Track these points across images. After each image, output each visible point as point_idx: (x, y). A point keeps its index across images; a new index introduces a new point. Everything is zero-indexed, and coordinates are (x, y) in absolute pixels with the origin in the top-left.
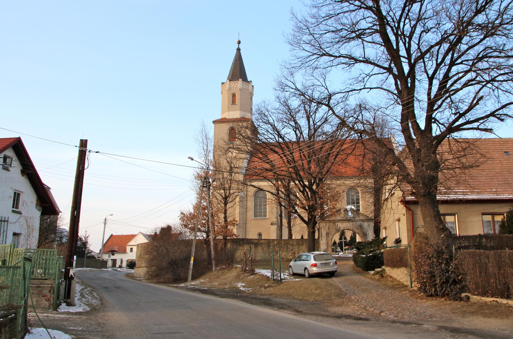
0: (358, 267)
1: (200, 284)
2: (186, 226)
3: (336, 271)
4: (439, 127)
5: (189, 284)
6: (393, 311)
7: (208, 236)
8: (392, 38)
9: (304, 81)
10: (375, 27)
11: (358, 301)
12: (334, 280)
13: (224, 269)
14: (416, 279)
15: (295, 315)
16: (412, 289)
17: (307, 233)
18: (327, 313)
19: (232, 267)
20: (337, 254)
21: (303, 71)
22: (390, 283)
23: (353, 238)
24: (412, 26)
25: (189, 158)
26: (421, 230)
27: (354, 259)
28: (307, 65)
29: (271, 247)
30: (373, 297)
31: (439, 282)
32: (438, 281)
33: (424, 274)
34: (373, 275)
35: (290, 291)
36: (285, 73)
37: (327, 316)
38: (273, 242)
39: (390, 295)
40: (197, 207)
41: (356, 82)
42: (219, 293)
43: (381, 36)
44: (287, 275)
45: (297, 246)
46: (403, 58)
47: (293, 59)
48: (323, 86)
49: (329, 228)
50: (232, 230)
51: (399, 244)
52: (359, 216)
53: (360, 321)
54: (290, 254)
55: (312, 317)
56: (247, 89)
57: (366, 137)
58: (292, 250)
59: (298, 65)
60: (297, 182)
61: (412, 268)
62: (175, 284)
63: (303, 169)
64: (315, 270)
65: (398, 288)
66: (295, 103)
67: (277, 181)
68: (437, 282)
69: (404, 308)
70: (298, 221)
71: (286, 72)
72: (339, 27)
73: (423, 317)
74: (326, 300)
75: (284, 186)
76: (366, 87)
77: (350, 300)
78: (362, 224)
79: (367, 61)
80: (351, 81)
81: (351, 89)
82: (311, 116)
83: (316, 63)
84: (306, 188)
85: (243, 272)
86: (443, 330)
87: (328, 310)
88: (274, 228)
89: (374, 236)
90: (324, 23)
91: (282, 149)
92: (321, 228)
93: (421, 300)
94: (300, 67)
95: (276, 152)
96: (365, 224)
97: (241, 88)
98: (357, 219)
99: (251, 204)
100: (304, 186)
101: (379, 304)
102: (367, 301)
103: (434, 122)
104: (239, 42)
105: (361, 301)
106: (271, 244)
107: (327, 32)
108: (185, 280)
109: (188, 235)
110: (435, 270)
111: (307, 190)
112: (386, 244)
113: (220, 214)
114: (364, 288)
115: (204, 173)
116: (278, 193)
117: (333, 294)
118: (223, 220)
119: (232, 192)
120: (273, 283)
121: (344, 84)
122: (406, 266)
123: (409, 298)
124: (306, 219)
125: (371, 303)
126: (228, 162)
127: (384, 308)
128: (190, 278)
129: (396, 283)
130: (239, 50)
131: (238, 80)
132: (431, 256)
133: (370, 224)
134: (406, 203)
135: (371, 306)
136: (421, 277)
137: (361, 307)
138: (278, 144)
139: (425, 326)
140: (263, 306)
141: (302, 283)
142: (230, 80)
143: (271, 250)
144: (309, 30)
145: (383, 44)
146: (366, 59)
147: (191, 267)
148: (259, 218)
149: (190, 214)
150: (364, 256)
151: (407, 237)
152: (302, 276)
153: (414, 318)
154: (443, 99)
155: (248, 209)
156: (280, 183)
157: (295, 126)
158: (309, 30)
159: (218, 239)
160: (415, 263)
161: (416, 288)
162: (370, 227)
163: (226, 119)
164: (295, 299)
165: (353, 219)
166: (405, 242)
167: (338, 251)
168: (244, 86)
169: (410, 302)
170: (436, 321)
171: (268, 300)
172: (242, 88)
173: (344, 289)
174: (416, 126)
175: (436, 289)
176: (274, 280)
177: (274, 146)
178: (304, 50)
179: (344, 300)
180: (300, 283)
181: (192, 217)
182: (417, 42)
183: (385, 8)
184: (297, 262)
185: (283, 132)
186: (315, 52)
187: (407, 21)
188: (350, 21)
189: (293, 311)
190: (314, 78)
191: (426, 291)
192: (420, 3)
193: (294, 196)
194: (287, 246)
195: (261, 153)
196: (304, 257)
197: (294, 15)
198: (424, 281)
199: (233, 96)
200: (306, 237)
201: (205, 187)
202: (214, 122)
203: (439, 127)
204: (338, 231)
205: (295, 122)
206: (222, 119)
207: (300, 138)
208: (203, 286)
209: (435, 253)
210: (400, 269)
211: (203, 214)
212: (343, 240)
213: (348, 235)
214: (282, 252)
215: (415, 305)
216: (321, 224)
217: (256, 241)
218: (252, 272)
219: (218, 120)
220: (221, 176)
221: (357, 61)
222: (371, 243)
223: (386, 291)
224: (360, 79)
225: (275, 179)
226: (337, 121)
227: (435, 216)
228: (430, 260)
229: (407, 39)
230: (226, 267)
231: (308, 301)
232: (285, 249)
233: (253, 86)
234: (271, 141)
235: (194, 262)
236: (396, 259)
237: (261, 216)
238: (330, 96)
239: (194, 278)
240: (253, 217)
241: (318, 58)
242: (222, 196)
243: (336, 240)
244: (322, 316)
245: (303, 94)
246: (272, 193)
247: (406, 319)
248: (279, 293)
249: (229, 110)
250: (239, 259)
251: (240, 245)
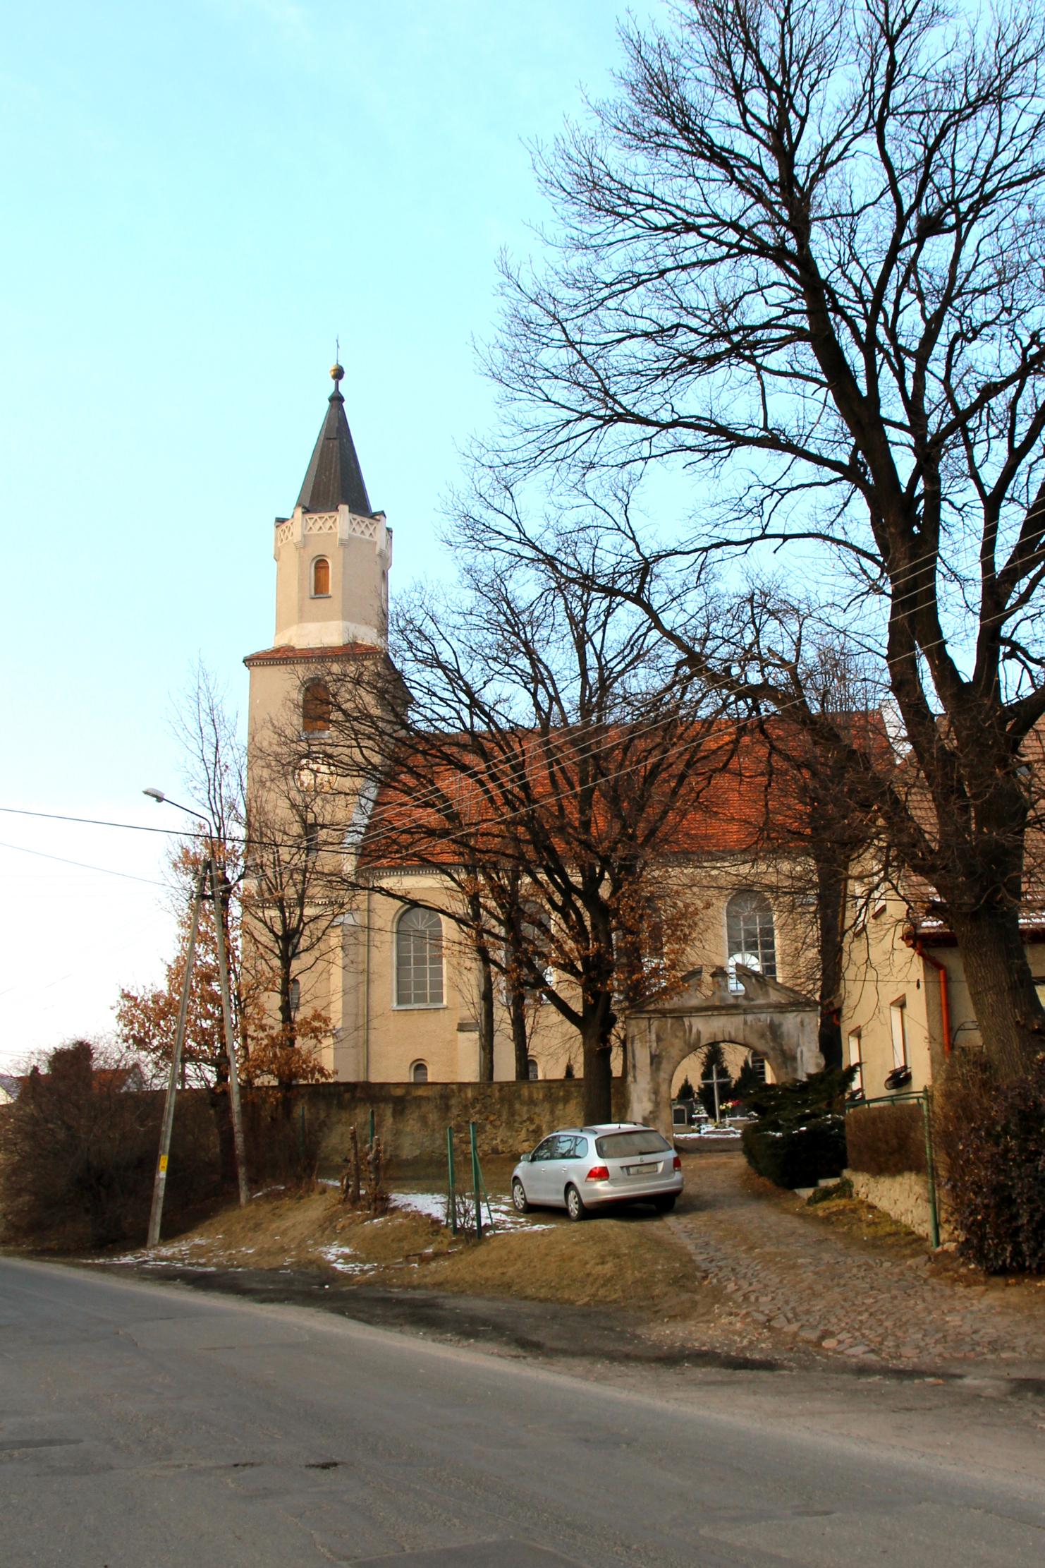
0: (761, 1174)
1: (192, 1255)
2: (141, 1043)
3: (677, 1193)
4: (1030, 671)
5: (152, 1254)
6: (867, 1332)
7: (222, 1077)
8: (855, 358)
9: (553, 513)
10: (792, 319)
11: (746, 1297)
12: (672, 1227)
13: (278, 1196)
14: (952, 1214)
15: (516, 1357)
16: (939, 1249)
17: (581, 1059)
18: (628, 1348)
19: (310, 1190)
20: (693, 1131)
21: (545, 474)
22: (865, 1230)
23: (752, 1074)
24: (928, 316)
25: (146, 793)
26: (974, 1038)
27: (746, 1146)
28: (560, 452)
29: (455, 1112)
30: (802, 1281)
31: (1029, 1222)
32: (1024, 1220)
33: (975, 1193)
34: (812, 1201)
35: (511, 1271)
36: (483, 482)
37: (627, 1358)
38: (460, 1091)
39: (862, 1273)
40: (182, 972)
41: (736, 515)
42: (254, 1285)
43: (818, 354)
44: (506, 1213)
45: (547, 1106)
46: (898, 431)
47: (509, 434)
48: (619, 529)
49: (659, 1039)
50: (310, 1052)
51: (904, 1090)
52: (767, 994)
53: (741, 1374)
54: (523, 1134)
55: (574, 1362)
56: (369, 542)
57: (768, 707)
58: (531, 1120)
59: (526, 455)
60: (542, 877)
61: (938, 1175)
62: (99, 1257)
63: (561, 830)
64: (604, 1190)
65: (892, 1246)
66: (757, 591)
67: (471, 870)
68: (1020, 1222)
69: (904, 1319)
70: (552, 1015)
71: (487, 481)
72: (669, 319)
73: (967, 1348)
74: (633, 1301)
75: (498, 892)
76: (768, 532)
77: (718, 1295)
78: (776, 1022)
79: (772, 440)
80: (714, 514)
81: (715, 541)
82: (590, 639)
83: (592, 446)
84: (574, 897)
85: (348, 1206)
86: (1030, 1395)
87: (638, 1337)
88: (470, 1041)
89: (822, 1062)
90: (611, 303)
91: (485, 755)
92: (633, 1037)
93: (968, 1286)
94: (533, 463)
95: (464, 768)
96: (790, 1022)
97: (346, 537)
98: (761, 1001)
99: (385, 954)
100: (568, 890)
101: (819, 1305)
102: (780, 1296)
103: (1008, 656)
104: (339, 374)
105: (757, 1299)
106: (453, 1102)
107: (624, 335)
108: (139, 1240)
109: (156, 1077)
110: (1012, 1179)
111: (579, 903)
112: (861, 1090)
113: (264, 997)
114: (773, 1249)
115: (206, 847)
116: (477, 916)
117: (659, 1276)
118: (279, 1016)
119: (309, 911)
120: (452, 1244)
121: (692, 523)
122: (916, 1166)
123: (925, 1281)
124: (577, 1007)
125: (792, 1304)
126: (293, 806)
127: (834, 1320)
128: (155, 1232)
129: (888, 1229)
130: (337, 400)
131: (337, 510)
132: (999, 1128)
133: (807, 1021)
134: (915, 939)
135: (790, 1315)
136: (968, 1206)
137: (754, 1321)
138: (467, 739)
139: (968, 1381)
140: (407, 1328)
141: (552, 1238)
142: (307, 511)
143: (453, 1123)
144: (564, 330)
145: (823, 378)
146: (770, 431)
147: (160, 1191)
148: (416, 1006)
149: (156, 998)
150: (778, 1134)
151: (928, 1062)
152: (556, 1212)
153: (935, 1353)
154: (1031, 575)
155: (373, 977)
156: (481, 878)
157: (530, 671)
158: (564, 330)
159: (259, 1088)
160: (949, 1154)
161: (951, 1246)
162: (808, 1029)
163: (292, 649)
164: (526, 1298)
165: (744, 1002)
166: (921, 1078)
167: (698, 1120)
168: (359, 530)
169: (928, 1296)
170: (1009, 1363)
171: (430, 1304)
172: (351, 538)
173: (699, 1258)
174: (945, 670)
175: (1017, 1246)
176: (456, 1231)
177: (457, 744)
178: (549, 400)
179: (698, 1297)
180: (546, 1240)
181: (162, 1010)
182: (942, 375)
183: (834, 251)
184: (538, 1164)
185: (487, 696)
186: (585, 409)
187: (907, 297)
188: (712, 299)
189: (507, 1344)
190: (585, 501)
191: (985, 1257)
192: (954, 234)
193: (532, 923)
194: (511, 1106)
195: (411, 771)
196: (564, 1147)
197: (509, 276)
198: (975, 1220)
199: (316, 568)
200: (579, 1073)
201: (207, 897)
202: (249, 661)
203: (1030, 671)
204: (693, 1047)
205: (531, 659)
206: (277, 650)
207: (548, 714)
208: (202, 1261)
209: (1014, 1120)
210: (899, 1179)
211: (202, 997)
212: (714, 1079)
213: (735, 1060)
214: (495, 1127)
215: (945, 1307)
216: (633, 1022)
217: (399, 1092)
218: (381, 1205)
219: (265, 652)
220: (268, 857)
221: (738, 440)
222: (804, 1088)
223: (849, 1261)
224: (748, 503)
225: (466, 867)
226: (672, 655)
227: (1013, 988)
228: (997, 1145)
229: (910, 364)
230: (288, 1189)
231: (572, 1303)
232: (504, 1117)
233: (389, 530)
234: (448, 730)
235: (168, 1174)
236: (887, 1142)
237: (421, 998)
238: (645, 569)
239: (169, 1234)
240: (395, 1004)
241: (596, 429)
242: (272, 931)
243: (691, 1081)
244: (612, 1357)
245: (550, 561)
246: (460, 921)
247: (910, 1356)
248: (469, 1278)
249: (302, 617)
250: (338, 1159)
251: (341, 1106)
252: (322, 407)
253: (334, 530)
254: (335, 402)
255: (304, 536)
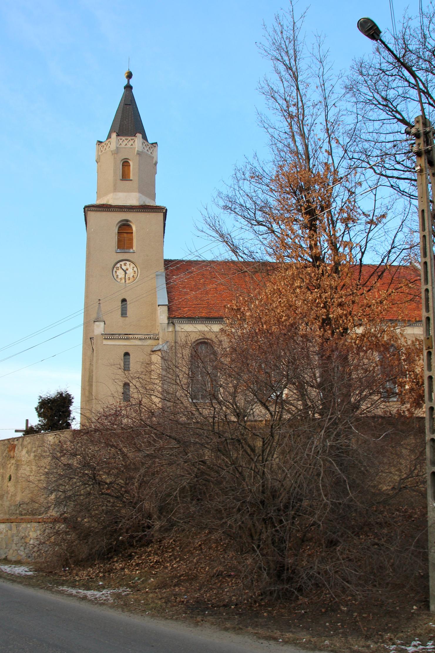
56: (150, 156)
104: (130, 76)
130: (129, 88)
202: (88, 209)
249: (115, 189)
252: (121, 92)
253: (134, 146)
254: (129, 89)
255: (117, 148)
